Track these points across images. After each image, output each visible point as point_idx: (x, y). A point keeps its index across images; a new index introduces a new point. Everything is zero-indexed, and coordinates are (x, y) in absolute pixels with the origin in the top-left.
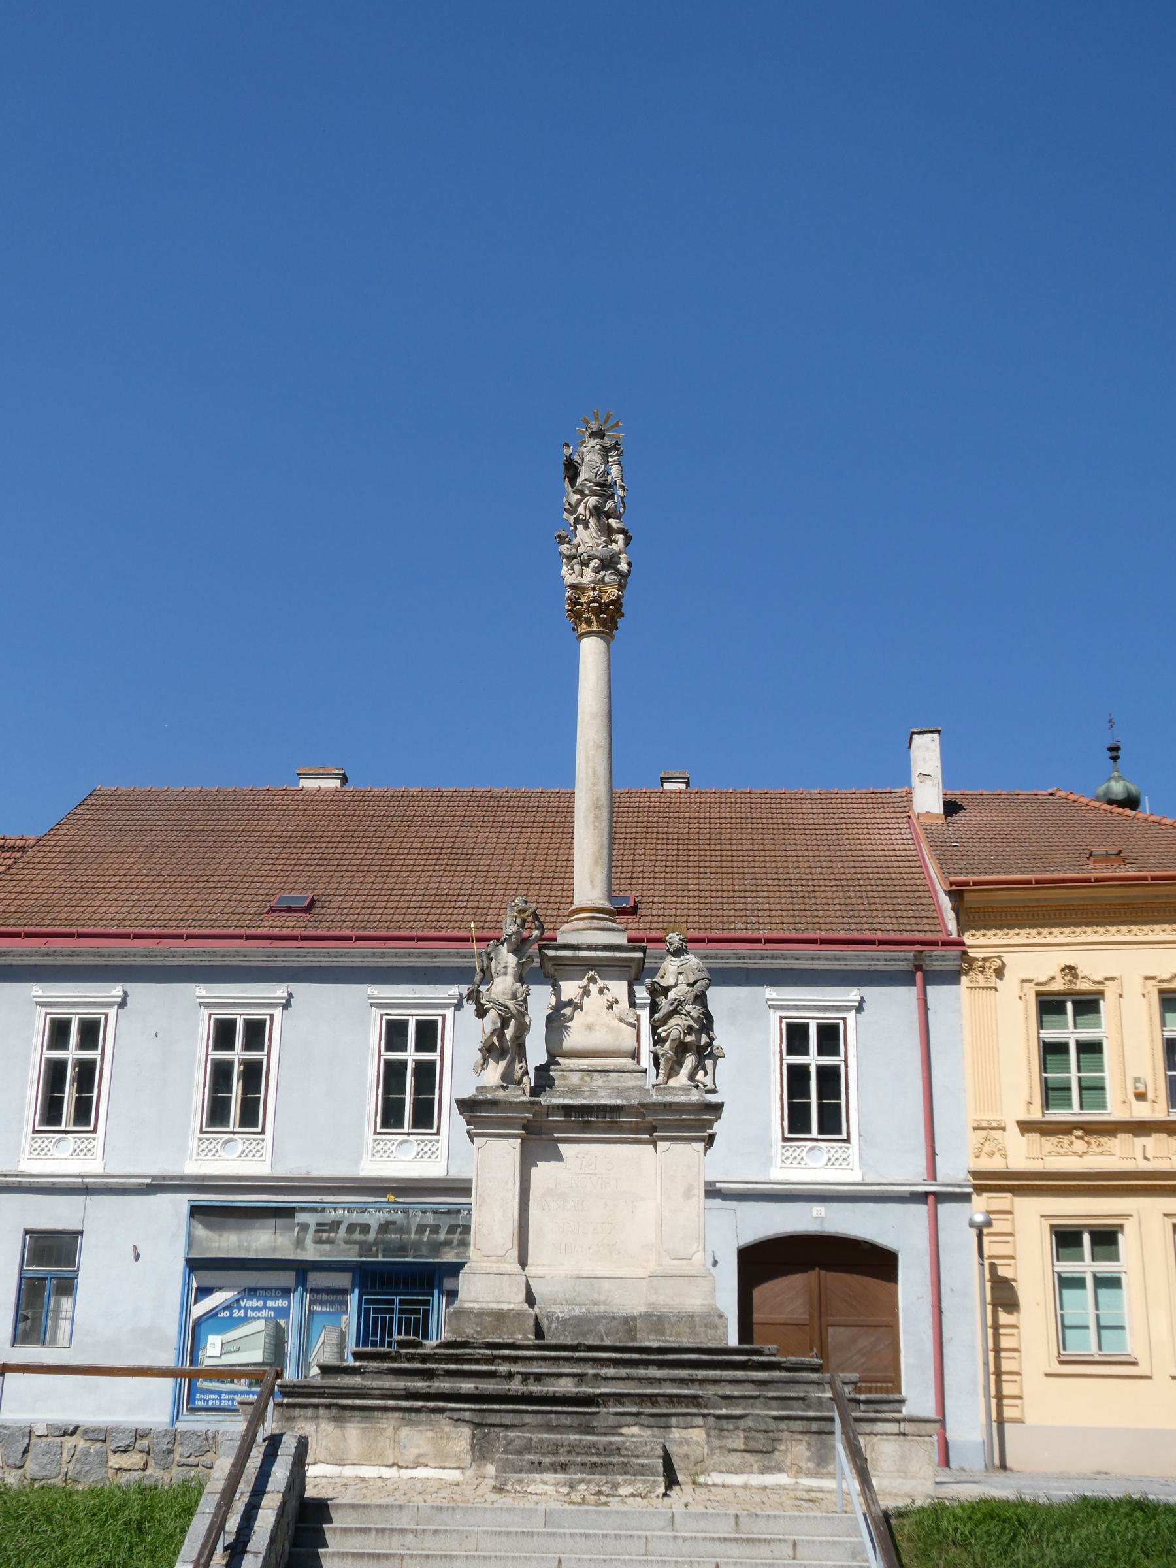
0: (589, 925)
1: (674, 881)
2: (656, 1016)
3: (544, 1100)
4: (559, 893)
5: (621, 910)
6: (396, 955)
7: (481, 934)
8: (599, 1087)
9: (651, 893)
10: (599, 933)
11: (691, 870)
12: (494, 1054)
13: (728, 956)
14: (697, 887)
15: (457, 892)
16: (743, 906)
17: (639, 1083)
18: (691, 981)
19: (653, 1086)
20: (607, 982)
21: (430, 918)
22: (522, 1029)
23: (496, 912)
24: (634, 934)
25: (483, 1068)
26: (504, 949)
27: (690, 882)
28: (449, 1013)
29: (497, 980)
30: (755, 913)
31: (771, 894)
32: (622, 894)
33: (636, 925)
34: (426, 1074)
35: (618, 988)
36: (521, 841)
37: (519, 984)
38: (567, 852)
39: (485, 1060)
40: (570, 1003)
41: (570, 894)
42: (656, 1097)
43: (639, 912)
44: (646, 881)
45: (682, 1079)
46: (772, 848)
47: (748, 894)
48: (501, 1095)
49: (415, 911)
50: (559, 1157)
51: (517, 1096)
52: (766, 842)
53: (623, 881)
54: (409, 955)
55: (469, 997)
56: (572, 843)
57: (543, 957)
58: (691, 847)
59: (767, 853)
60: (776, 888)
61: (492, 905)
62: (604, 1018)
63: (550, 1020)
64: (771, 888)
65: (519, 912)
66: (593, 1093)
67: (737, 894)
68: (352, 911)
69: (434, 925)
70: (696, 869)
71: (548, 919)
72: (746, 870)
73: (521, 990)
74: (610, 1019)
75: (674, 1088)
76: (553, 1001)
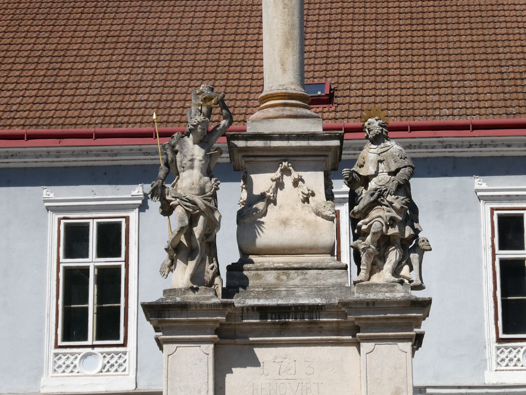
0: (280, 113)
1: (372, 66)
2: (356, 208)
3: (238, 301)
4: (248, 83)
5: (314, 98)
6: (73, 154)
7: (164, 128)
8: (297, 286)
9: (347, 80)
10: (292, 121)
11: (391, 53)
12: (183, 253)
13: (433, 145)
14: (397, 72)
15: (137, 84)
16: (449, 91)
17: (339, 280)
18: (393, 169)
19: (355, 283)
20: (301, 173)
21: (109, 112)
22: (213, 226)
23: (181, 104)
24: (330, 124)
25: (171, 270)
26: (189, 140)
27: (391, 65)
28: (133, 215)
29: (183, 175)
30: (462, 97)
31: (479, 77)
32: (316, 81)
33: (332, 115)
34: (111, 282)
35: (315, 180)
36: (206, 26)
37: (207, 178)
38: (256, 37)
39: (173, 262)
40: (262, 197)
41: (260, 83)
42: (358, 295)
43: (335, 100)
44: (342, 66)
45: (385, 275)
46: (480, 25)
47: (454, 77)
48: (191, 297)
49: (92, 106)
50: (256, 363)
51: (208, 298)
52: (473, 20)
53: (317, 68)
54: (88, 153)
55: (153, 193)
56: (261, 28)
57: (232, 149)
58: (390, 28)
59: (474, 32)
60: (485, 70)
61: (176, 97)
62: (299, 213)
63: (241, 216)
64: (479, 70)
65: (205, 100)
66: (290, 293)
67: (441, 78)
68: (22, 107)
69: (113, 120)
70: (397, 52)
71: (237, 111)
72: (451, 51)
73: (209, 185)
74: (306, 213)
75: (377, 285)
76: (244, 195)
